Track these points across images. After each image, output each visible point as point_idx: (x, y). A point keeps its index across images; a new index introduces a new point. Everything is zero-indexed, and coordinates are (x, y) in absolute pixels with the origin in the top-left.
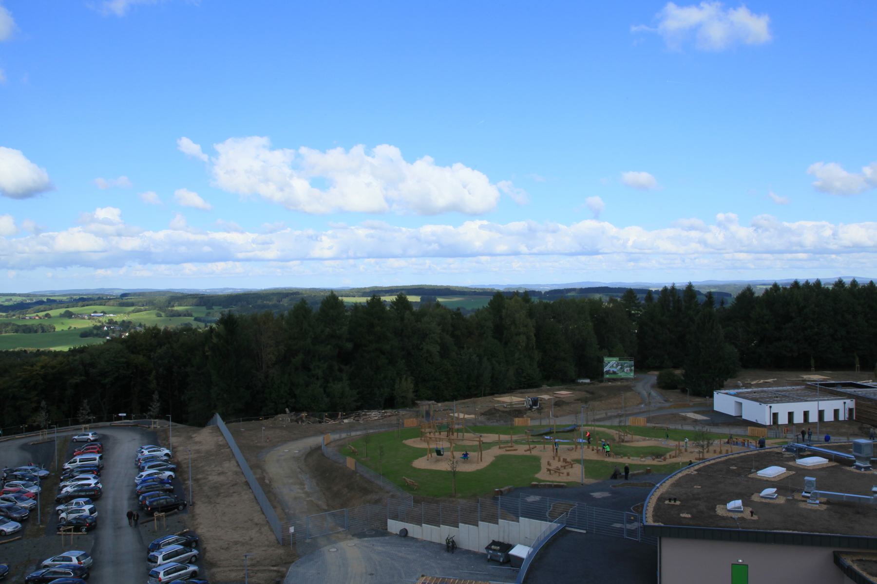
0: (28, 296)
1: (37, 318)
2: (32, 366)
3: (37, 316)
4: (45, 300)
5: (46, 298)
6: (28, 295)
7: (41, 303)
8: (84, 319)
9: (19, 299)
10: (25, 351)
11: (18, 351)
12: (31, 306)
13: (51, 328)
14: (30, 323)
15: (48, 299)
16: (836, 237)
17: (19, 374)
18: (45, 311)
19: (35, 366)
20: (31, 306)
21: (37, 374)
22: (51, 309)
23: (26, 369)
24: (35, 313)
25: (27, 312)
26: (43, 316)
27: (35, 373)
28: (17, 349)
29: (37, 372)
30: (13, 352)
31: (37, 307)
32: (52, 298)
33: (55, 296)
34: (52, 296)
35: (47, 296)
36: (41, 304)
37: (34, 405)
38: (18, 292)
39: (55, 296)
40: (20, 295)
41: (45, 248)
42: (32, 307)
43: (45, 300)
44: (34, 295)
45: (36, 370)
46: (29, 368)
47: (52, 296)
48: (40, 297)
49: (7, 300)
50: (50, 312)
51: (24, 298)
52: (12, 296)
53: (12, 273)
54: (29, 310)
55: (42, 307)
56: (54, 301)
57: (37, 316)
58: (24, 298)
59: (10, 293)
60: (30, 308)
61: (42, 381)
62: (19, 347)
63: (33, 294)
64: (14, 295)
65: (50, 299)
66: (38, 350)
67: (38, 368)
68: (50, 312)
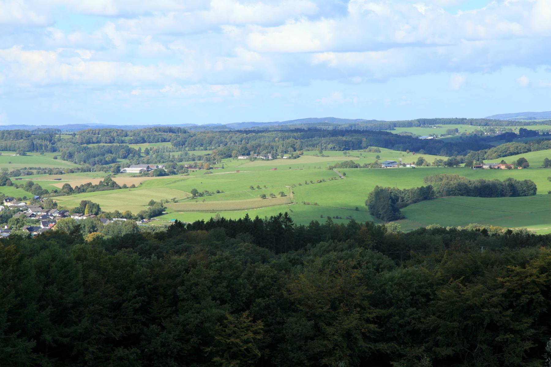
0: (486, 125)
1: (503, 167)
2: (523, 265)
3: (503, 162)
4: (517, 132)
5: (519, 128)
6: (485, 122)
7: (509, 137)
8: (216, 164)
9: (469, 130)
10: (485, 231)
11: (430, 229)
12: (492, 144)
13: (528, 187)
14: (490, 178)
15: (521, 130)
16: (97, 132)
17: (500, 279)
18: (517, 153)
19: (528, 267)
20: (492, 144)
21: (534, 282)
22: (529, 150)
23: (512, 271)
24: (500, 156)
25: (485, 156)
26: (514, 163)
27: (528, 280)
28: (469, 227)
29: (534, 278)
30: (464, 233)
31: (503, 146)
32: (529, 128)
33: (535, 123)
34: (528, 124)
35: (520, 123)
36: (510, 141)
37: (528, 345)
38: (468, 117)
39: (535, 123)
40: (472, 122)
41: (516, 28)
42: (495, 147)
43: (517, 132)
44: (498, 122)
45: (531, 275)
46: (518, 269)
47: (528, 124)
48: (508, 125)
49: (449, 132)
50: (527, 156)
51: (479, 128)
52: (459, 123)
53: (459, 79)
54: (489, 151)
55: (512, 146)
56: (534, 133)
57: (503, 162)
58: (479, 128)
59: (454, 117)
60: (490, 147)
61: (542, 298)
62: (472, 223)
63: (495, 121)
64: (462, 121)
65: (525, 129)
66: (510, 232)
67: (535, 271)
68: (527, 156)
